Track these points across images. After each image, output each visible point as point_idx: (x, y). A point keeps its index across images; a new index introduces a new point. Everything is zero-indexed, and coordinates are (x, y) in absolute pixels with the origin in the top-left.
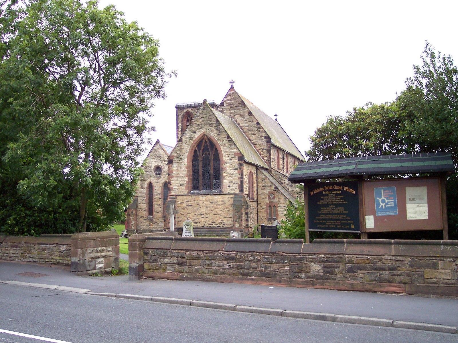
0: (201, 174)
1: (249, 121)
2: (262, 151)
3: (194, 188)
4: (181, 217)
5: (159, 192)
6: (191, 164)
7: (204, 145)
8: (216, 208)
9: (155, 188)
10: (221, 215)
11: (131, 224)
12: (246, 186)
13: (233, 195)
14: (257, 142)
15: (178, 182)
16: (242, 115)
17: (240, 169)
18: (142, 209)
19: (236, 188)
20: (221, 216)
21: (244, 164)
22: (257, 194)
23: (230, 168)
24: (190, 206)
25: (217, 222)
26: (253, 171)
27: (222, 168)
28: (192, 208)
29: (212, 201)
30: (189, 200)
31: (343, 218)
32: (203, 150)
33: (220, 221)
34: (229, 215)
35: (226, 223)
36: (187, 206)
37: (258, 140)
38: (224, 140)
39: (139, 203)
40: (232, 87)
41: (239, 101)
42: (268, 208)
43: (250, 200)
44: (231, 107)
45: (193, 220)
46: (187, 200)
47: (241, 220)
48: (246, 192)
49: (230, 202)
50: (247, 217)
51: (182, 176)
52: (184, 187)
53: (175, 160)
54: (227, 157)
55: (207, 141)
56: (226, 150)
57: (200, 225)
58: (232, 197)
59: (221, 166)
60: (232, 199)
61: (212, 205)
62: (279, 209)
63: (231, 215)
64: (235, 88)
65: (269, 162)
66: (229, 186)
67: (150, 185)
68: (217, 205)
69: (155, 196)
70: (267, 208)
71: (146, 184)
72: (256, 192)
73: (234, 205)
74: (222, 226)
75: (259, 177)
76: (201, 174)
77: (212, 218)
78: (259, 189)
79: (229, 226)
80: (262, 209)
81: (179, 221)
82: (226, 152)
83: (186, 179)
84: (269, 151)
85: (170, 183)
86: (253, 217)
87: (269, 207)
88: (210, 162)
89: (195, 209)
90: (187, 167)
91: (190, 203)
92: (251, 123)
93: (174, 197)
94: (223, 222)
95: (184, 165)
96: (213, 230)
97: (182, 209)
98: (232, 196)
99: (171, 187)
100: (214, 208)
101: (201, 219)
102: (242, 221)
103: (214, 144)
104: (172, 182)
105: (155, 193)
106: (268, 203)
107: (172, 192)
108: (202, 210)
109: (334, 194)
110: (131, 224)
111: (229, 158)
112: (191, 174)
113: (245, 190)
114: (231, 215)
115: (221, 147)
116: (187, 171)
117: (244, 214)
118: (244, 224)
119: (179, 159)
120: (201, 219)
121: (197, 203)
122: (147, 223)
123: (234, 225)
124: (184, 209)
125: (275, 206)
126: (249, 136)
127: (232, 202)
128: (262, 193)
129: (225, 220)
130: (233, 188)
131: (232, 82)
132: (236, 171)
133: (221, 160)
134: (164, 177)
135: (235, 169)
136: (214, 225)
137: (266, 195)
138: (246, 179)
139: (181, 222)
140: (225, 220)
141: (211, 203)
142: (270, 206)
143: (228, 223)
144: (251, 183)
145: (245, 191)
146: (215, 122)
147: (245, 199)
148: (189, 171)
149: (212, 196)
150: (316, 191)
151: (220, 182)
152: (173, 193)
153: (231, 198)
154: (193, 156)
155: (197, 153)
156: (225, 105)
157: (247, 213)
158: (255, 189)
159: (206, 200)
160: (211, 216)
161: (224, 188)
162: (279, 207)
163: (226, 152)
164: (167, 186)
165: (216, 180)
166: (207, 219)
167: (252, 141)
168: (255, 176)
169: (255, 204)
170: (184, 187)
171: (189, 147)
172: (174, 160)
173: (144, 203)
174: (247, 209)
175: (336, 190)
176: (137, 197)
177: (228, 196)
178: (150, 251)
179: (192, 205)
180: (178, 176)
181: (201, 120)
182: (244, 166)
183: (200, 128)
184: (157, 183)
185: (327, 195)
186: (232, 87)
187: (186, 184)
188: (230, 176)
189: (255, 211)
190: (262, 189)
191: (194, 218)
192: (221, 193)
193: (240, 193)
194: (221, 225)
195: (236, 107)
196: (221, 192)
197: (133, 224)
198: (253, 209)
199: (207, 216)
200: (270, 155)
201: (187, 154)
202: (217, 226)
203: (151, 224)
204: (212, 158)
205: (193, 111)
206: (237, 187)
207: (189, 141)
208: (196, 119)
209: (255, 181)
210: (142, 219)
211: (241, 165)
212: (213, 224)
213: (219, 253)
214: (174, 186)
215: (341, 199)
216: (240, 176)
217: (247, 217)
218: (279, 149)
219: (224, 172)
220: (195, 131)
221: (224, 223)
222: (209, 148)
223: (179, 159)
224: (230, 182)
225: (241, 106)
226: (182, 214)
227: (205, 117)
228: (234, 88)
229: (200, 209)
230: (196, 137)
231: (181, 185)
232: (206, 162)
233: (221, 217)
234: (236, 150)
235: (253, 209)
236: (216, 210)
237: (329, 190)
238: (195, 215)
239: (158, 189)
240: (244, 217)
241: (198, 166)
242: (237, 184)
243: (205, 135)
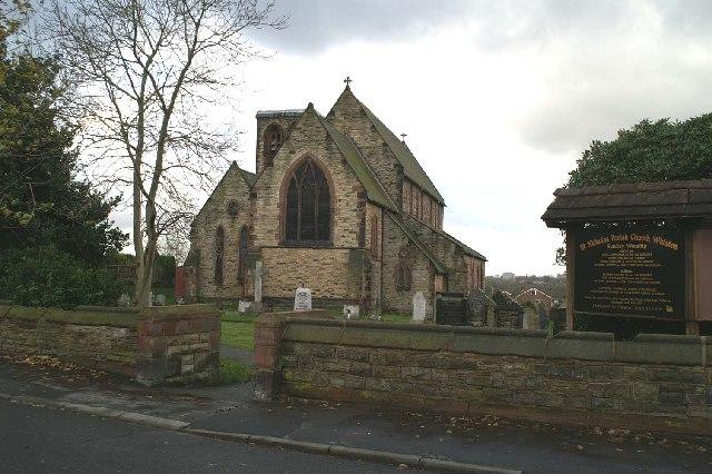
12: (368, 236)
16: (362, 131)
25: (322, 291)
31: (151, 276)
35: (336, 292)
40: (348, 88)
41: (357, 109)
50: (369, 284)
53: (261, 193)
61: (315, 264)
65: (400, 201)
67: (220, 230)
71: (214, 226)
78: (386, 242)
84: (400, 186)
85: (251, 228)
91: (281, 261)
98: (345, 251)
109: (632, 249)
131: (348, 80)
132: (355, 214)
134: (242, 220)
143: (339, 292)
144: (374, 231)
148: (282, 211)
150: (592, 244)
152: (256, 243)
157: (368, 278)
158: (380, 242)
164: (246, 233)
169: (378, 264)
175: (636, 243)
177: (341, 251)
178: (298, 347)
185: (617, 250)
186: (348, 88)
192: (330, 246)
200: (401, 191)
205: (285, 125)
211: (361, 205)
213: (440, 356)
215: (647, 258)
217: (369, 284)
218: (409, 180)
234: (357, 184)
237: (620, 243)
239: (232, 236)
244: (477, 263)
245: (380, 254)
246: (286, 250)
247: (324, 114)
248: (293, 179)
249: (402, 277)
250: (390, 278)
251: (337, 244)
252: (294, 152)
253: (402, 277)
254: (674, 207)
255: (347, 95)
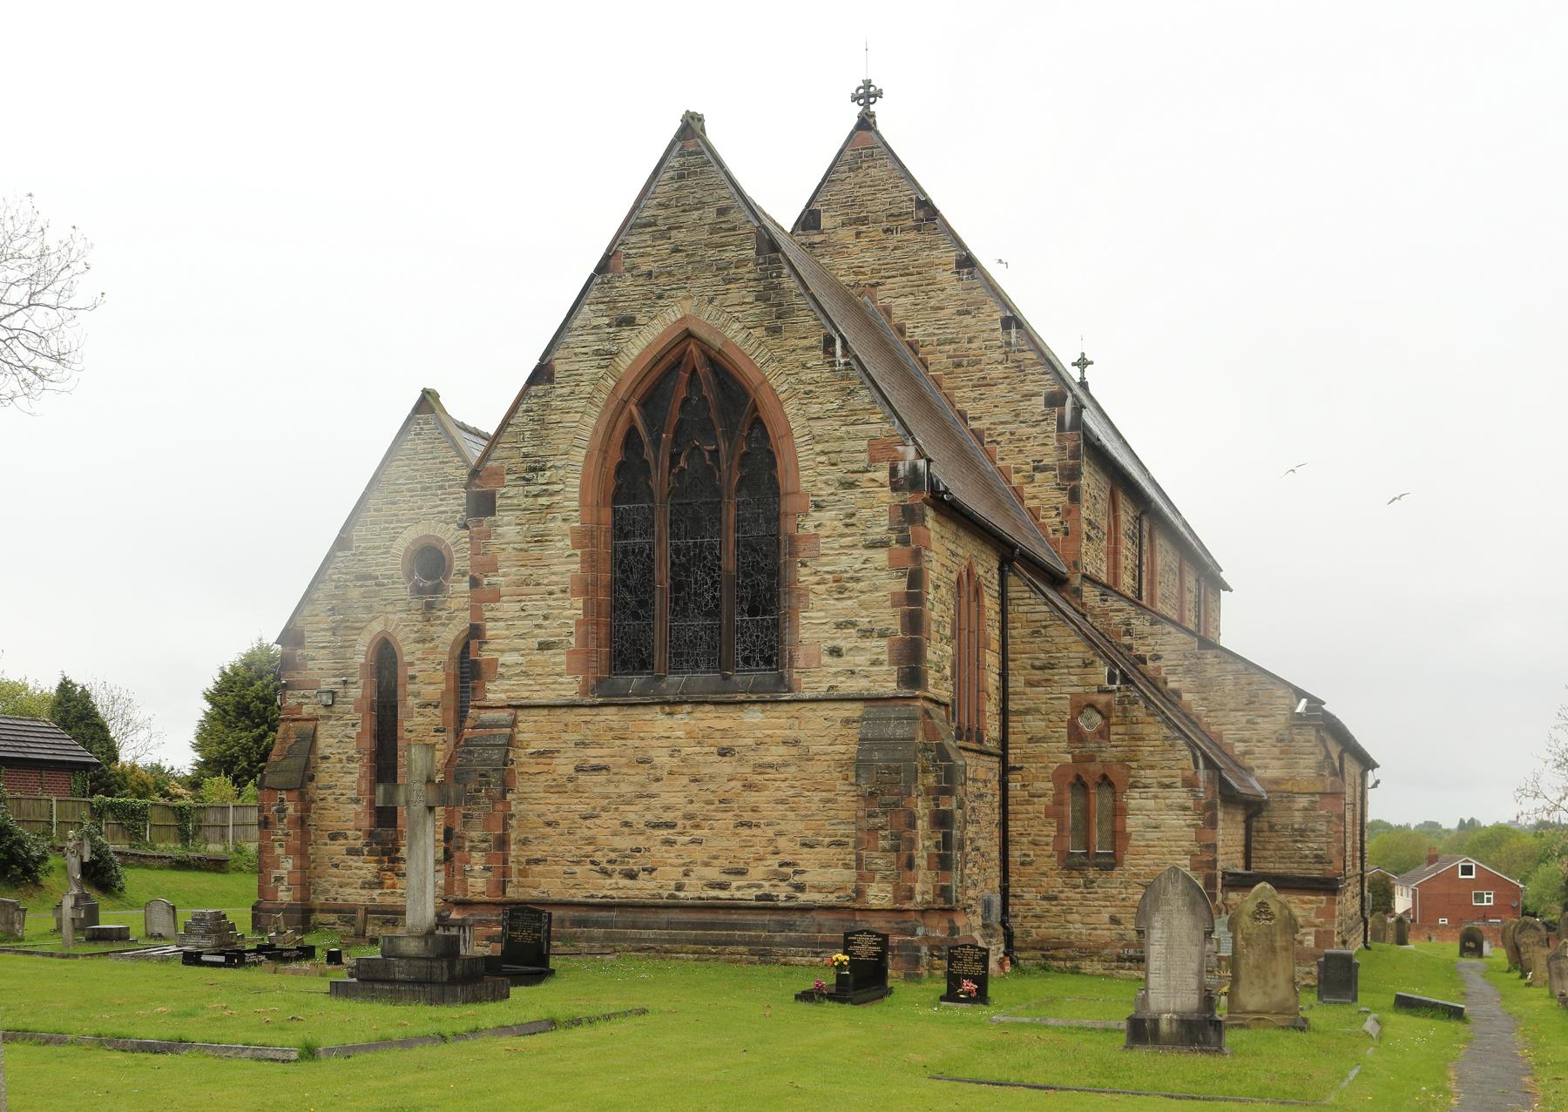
0: (662, 576)
1: (959, 313)
2: (1031, 479)
3: (624, 664)
4: (544, 837)
5: (433, 691)
6: (606, 515)
7: (686, 401)
8: (749, 786)
9: (411, 671)
10: (782, 827)
11: (276, 873)
12: (938, 652)
13: (859, 706)
14: (1000, 428)
15: (523, 625)
17: (904, 541)
18: (338, 792)
19: (874, 663)
20: (780, 834)
21: (930, 513)
22: (1004, 713)
23: (842, 536)
24: (597, 769)
25: (757, 873)
26: (980, 571)
27: (793, 540)
28: (609, 781)
29: (726, 743)
30: (588, 733)
32: (679, 430)
33: (773, 862)
34: (829, 829)
36: (578, 769)
37: (1008, 418)
38: (804, 366)
39: (325, 758)
40: (866, 123)
42: (1068, 795)
43: (960, 743)
44: (858, 235)
45: (613, 855)
46: (577, 737)
47: (904, 859)
48: (939, 686)
49: (842, 748)
50: (946, 843)
51: (551, 593)
52: (559, 658)
53: (511, 493)
54: (820, 469)
55: (704, 371)
56: (817, 427)
57: (652, 884)
58: (847, 714)
59: (788, 526)
60: (854, 732)
61: (726, 767)
62: (1134, 800)
63: (842, 829)
64: (883, 125)
66: (836, 652)
68: (761, 768)
69: (410, 716)
70: (1059, 793)
72: (995, 695)
73: (860, 765)
74: (789, 898)
75: (1017, 611)
76: (662, 576)
77: (726, 844)
78: (1016, 683)
79: (832, 899)
80: (1028, 802)
81: (528, 862)
82: (816, 439)
83: (574, 608)
86: (980, 843)
87: (1073, 786)
88: (716, 508)
89: (625, 788)
90: (584, 538)
91: (593, 755)
92: (967, 319)
93: (504, 715)
94: (790, 870)
95: (565, 526)
96: (735, 917)
97: (549, 789)
98: (854, 710)
99: (485, 656)
100: (738, 784)
101: (659, 852)
102: (910, 864)
103: (747, 395)
104: (489, 625)
105: (412, 702)
106: (1063, 766)
107: (489, 686)
108: (667, 799)
110: (276, 873)
111: (836, 474)
112: (606, 577)
113: (932, 676)
114: (842, 829)
115: (790, 408)
116: (582, 562)
117: (922, 824)
118: (923, 886)
119: (535, 489)
120: (659, 852)
121: (640, 755)
122: (366, 868)
123: (859, 892)
124: (559, 789)
125: (1111, 785)
126: (958, 393)
127: (854, 748)
128: (1030, 704)
129: (806, 858)
130: (861, 660)
132: (881, 556)
133: (785, 485)
135: (873, 545)
136: (740, 891)
137: (1052, 717)
138: (938, 608)
139: (540, 868)
140: (806, 858)
141: (724, 752)
142: (1080, 785)
144: (965, 634)
145: (931, 681)
146: (752, 253)
147: (931, 732)
148: (590, 562)
149: (724, 711)
151: (776, 625)
153: (847, 722)
154: (621, 469)
155: (640, 455)
156: (825, 222)
157: (942, 820)
159: (690, 735)
160: (721, 839)
161: (800, 663)
162: (1133, 786)
163: (816, 439)
165: (753, 611)
166: (698, 853)
167: (975, 425)
168: (991, 604)
170: (563, 658)
171: (595, 412)
172: (503, 496)
173: (350, 759)
174: (948, 792)
176: (311, 725)
179: (606, 768)
180: (525, 589)
181: (665, 247)
182: (930, 523)
183: (660, 297)
184: (424, 641)
186: (866, 123)
187: (572, 640)
188: (840, 585)
189: (989, 811)
190: (1029, 684)
191: (618, 842)
193: (905, 692)
194: (782, 892)
195: (886, 231)
196: (782, 683)
197: (283, 872)
198: (981, 796)
199: (697, 833)
200: (1074, 496)
201: (579, 456)
202: (758, 898)
203: (389, 879)
204: (729, 473)
206: (884, 657)
207: (595, 382)
208: (633, 239)
209: (994, 633)
210: (338, 848)
211: (909, 515)
212: (734, 884)
214: (503, 651)
216: (901, 586)
217: (946, 843)
219: (804, 565)
220: (628, 312)
221: (798, 879)
222: (713, 415)
223: (535, 489)
224: (839, 626)
225: (918, 229)
226: (551, 818)
227: (695, 227)
228: (881, 127)
229: (654, 788)
230: (636, 352)
231: (544, 646)
232: (694, 515)
233: (782, 843)
235: (981, 796)
236: (752, 797)
238: (626, 824)
240: (924, 841)
241: (648, 531)
242: (882, 635)
243: (688, 335)
244: (1351, 768)
245: (992, 730)
246: (610, 715)
247: (784, 210)
248: (632, 433)
249: (1085, 816)
250: (1036, 828)
251: (810, 682)
252: (629, 321)
253: (1085, 816)
254: (446, 1030)
255: (865, 146)
